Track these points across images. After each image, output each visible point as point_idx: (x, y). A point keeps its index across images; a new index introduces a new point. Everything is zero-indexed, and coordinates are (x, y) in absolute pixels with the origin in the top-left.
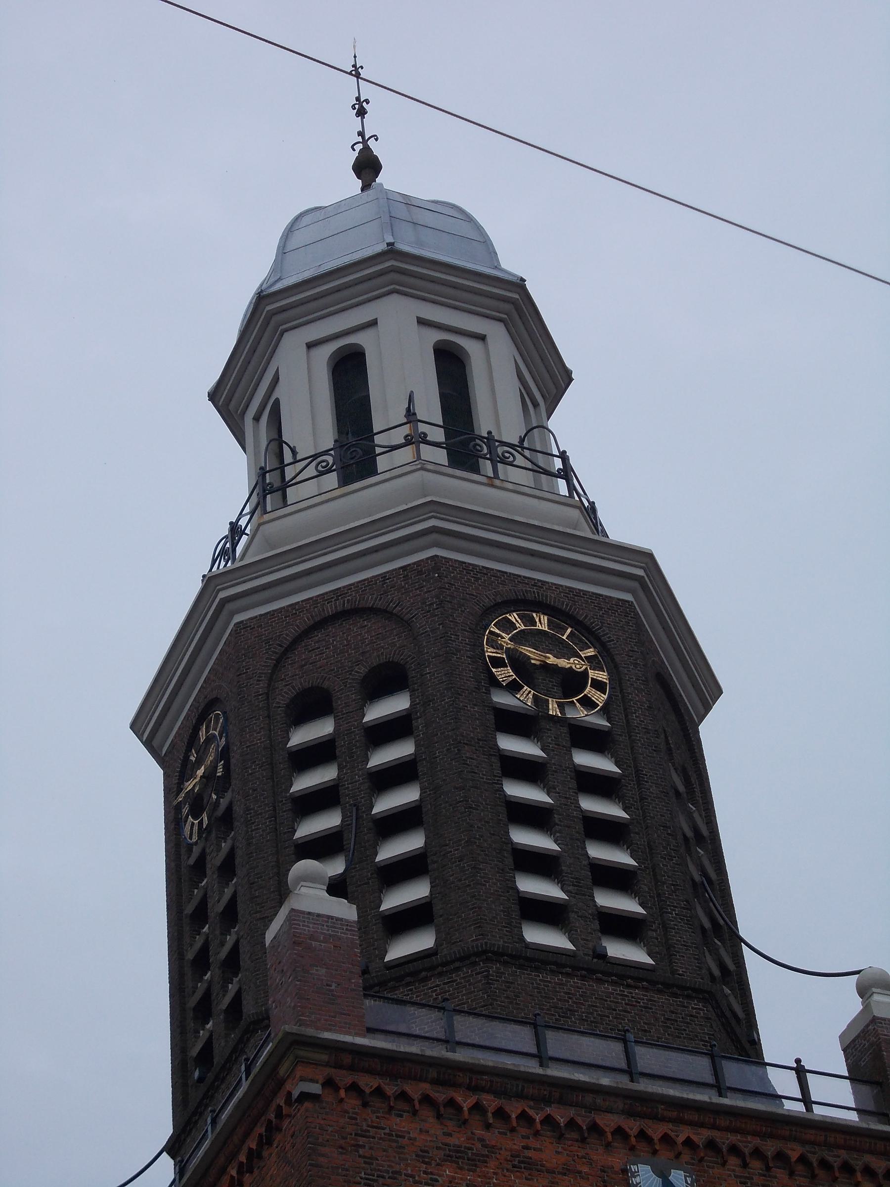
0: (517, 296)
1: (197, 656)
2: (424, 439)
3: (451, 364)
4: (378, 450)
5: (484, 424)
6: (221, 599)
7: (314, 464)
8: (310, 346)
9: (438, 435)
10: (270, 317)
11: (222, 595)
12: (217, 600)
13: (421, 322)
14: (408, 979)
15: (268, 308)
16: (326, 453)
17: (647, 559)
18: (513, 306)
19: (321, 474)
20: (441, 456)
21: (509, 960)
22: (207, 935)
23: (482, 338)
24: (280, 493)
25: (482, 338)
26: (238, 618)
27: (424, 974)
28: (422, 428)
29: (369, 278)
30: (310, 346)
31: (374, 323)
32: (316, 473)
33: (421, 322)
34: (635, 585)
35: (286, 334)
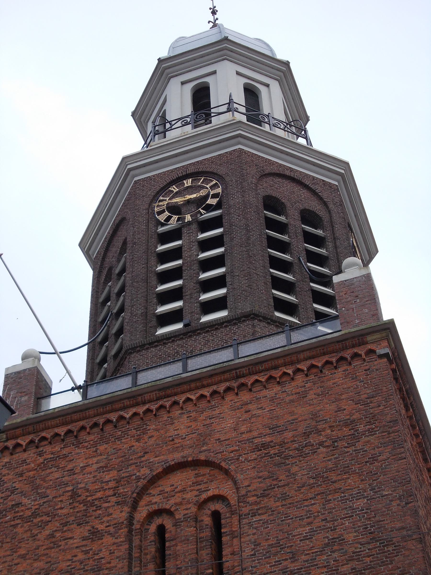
0: (285, 69)
1: (118, 195)
2: (236, 110)
3: (251, 94)
4: (212, 115)
5: (266, 110)
6: (128, 169)
7: (181, 121)
8: (183, 83)
9: (243, 110)
10: (165, 70)
11: (129, 167)
12: (126, 169)
13: (238, 73)
14: (261, 318)
15: (163, 66)
16: (188, 116)
17: (346, 165)
18: (283, 72)
19: (183, 126)
20: (244, 119)
21: (279, 325)
22: (109, 306)
23: (268, 86)
24: (163, 134)
25: (268, 86)
26: (136, 179)
27: (139, 348)
28: (235, 106)
29: (213, 52)
30: (183, 83)
31: (214, 72)
32: (181, 125)
33: (238, 73)
34: (340, 178)
35: (172, 79)
